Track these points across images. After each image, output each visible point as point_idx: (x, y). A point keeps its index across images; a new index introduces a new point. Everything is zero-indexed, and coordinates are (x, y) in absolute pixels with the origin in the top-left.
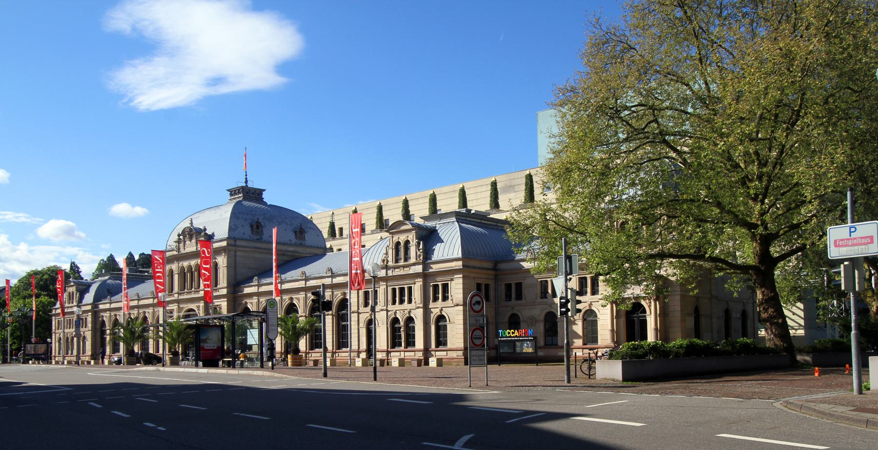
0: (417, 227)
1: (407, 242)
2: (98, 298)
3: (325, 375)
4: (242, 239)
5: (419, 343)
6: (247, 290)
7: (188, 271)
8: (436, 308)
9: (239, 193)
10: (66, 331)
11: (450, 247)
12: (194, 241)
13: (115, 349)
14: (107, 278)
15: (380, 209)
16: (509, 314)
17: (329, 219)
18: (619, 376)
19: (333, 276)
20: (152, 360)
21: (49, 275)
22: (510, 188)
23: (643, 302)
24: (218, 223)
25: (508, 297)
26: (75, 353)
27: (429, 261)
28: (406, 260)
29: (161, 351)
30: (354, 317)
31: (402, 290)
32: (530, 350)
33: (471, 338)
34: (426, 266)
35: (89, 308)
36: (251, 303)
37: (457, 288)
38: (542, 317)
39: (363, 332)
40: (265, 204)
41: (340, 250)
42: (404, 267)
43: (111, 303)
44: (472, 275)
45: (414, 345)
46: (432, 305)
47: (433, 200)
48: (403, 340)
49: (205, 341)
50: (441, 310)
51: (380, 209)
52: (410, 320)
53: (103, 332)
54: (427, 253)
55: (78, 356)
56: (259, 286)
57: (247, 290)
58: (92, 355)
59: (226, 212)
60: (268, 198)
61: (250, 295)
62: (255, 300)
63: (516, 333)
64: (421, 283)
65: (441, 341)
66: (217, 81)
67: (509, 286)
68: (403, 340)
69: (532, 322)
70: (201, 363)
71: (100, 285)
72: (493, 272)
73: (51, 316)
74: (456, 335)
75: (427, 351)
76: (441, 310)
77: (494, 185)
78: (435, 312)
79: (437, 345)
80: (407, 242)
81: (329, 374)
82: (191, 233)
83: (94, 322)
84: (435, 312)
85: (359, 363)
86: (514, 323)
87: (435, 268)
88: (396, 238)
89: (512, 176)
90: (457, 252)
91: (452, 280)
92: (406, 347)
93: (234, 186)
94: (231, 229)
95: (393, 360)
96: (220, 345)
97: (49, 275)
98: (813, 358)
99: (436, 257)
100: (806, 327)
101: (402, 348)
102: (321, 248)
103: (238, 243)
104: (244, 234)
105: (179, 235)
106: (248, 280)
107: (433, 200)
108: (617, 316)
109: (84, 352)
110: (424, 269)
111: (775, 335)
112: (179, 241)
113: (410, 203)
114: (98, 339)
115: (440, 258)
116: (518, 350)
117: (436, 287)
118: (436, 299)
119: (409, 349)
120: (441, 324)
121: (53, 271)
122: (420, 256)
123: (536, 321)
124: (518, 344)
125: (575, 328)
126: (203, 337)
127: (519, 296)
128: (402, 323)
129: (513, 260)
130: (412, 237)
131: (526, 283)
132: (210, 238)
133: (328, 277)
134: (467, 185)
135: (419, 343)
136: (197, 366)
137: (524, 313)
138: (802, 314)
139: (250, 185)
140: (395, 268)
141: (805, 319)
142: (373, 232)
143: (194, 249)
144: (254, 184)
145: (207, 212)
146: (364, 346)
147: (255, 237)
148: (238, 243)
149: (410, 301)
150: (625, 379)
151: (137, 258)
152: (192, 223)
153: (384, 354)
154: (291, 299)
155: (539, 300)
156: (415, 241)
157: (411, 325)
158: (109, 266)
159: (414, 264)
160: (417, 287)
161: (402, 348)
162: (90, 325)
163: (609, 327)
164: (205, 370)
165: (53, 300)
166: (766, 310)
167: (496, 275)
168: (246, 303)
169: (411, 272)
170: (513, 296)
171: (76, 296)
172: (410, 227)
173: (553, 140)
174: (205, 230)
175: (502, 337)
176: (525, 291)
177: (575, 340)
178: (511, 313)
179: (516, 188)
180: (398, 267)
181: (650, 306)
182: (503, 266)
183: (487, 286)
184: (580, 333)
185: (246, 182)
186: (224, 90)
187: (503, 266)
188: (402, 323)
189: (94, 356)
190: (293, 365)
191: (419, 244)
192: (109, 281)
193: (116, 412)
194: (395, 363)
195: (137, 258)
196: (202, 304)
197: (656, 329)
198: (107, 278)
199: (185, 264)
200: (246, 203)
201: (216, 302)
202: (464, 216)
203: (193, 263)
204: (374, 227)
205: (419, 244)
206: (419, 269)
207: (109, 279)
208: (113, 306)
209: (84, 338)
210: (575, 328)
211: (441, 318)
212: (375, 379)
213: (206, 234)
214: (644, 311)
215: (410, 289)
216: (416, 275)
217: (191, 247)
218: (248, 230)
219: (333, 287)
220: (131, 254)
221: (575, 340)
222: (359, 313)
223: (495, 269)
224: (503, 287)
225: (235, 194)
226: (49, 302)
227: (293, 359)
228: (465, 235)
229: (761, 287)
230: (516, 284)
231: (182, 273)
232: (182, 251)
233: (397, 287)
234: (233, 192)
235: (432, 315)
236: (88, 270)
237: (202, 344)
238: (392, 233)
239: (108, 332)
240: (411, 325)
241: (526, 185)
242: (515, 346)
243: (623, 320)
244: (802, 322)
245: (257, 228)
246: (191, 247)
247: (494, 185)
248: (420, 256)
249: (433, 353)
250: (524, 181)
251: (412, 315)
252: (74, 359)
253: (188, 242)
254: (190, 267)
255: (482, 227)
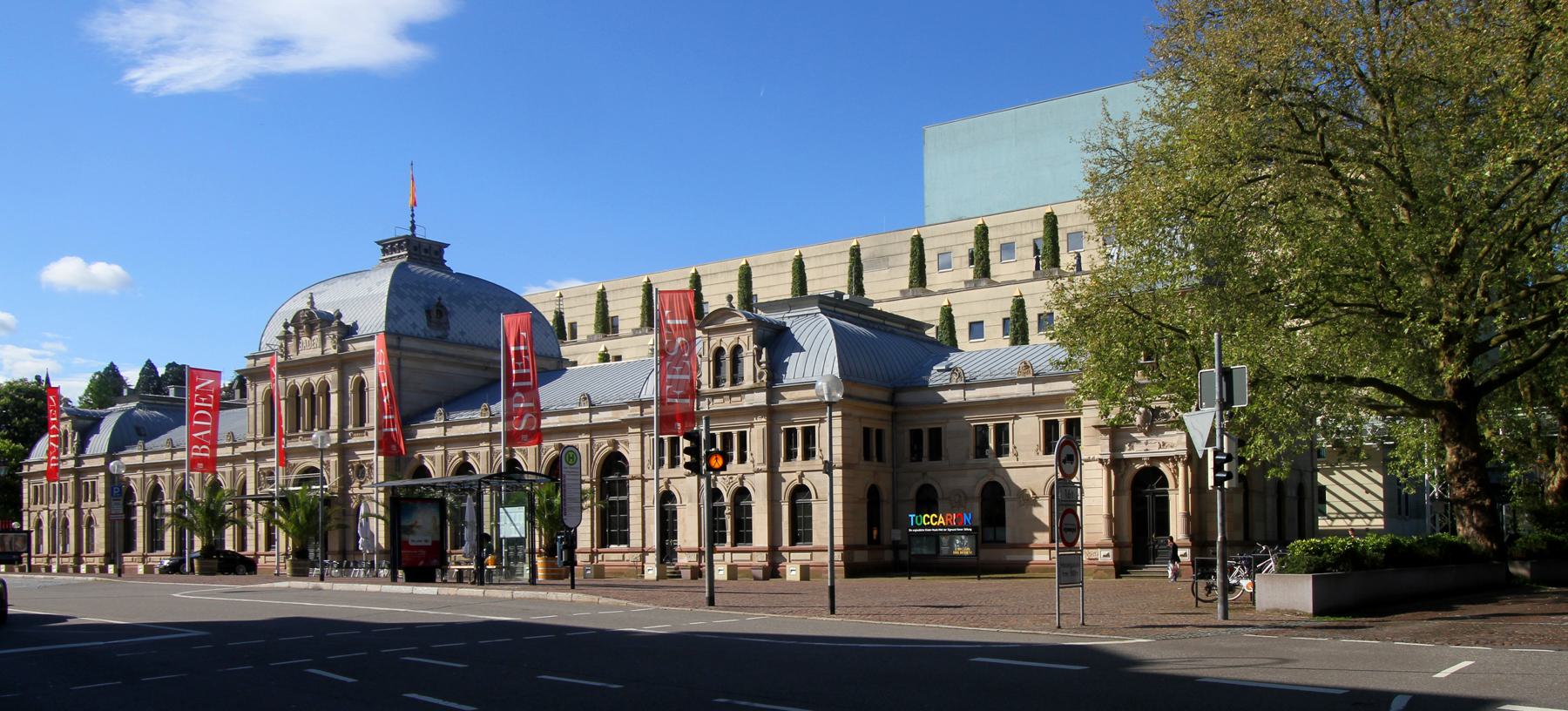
0: (758, 323)
1: (737, 349)
2: (117, 446)
3: (711, 602)
4: (412, 336)
5: (760, 536)
6: (423, 434)
7: (305, 395)
8: (791, 473)
9: (401, 248)
10: (54, 507)
11: (817, 362)
12: (317, 337)
13: (155, 544)
14: (133, 405)
15: (602, 296)
16: (917, 485)
17: (554, 307)
18: (1308, 606)
19: (593, 409)
20: (239, 565)
21: (12, 397)
22: (882, 260)
23: (1163, 467)
24: (365, 300)
25: (916, 455)
26: (71, 549)
27: (778, 385)
28: (734, 382)
29: (251, 549)
30: (634, 487)
31: (727, 438)
32: (967, 551)
33: (1060, 528)
34: (773, 395)
35: (101, 462)
36: (432, 458)
37: (831, 437)
38: (978, 492)
39: (652, 515)
40: (449, 271)
41: (618, 358)
42: (731, 394)
43: (145, 454)
44: (858, 413)
45: (749, 540)
46: (783, 466)
47: (746, 276)
48: (729, 530)
49: (409, 530)
50: (801, 476)
51: (602, 296)
52: (742, 493)
53: (130, 511)
54: (775, 370)
55: (78, 558)
56: (447, 425)
57: (423, 434)
58: (107, 555)
59: (379, 283)
60: (456, 260)
61: (430, 443)
62: (438, 452)
63: (941, 521)
64: (764, 426)
65: (801, 531)
66: (277, 45)
67: (916, 435)
68: (729, 530)
69: (958, 501)
70: (401, 573)
71: (118, 423)
72: (889, 409)
73: (21, 478)
74: (829, 520)
75: (774, 550)
76: (801, 476)
77: (855, 252)
78: (790, 480)
79: (794, 539)
80: (737, 349)
81: (717, 597)
82: (311, 321)
83: (110, 491)
84: (790, 480)
85: (651, 573)
86: (927, 501)
87: (790, 397)
88: (715, 341)
89: (884, 238)
90: (832, 367)
91: (1016, 417)
92: (734, 544)
93: (389, 234)
94: (390, 316)
95: (789, 567)
96: (437, 538)
97: (12, 397)
98: (1531, 571)
99: (790, 377)
100: (1387, 515)
101: (728, 545)
102: (552, 357)
103: (405, 343)
104: (414, 326)
105: (286, 325)
106: (424, 414)
107: (746, 276)
108: (1115, 492)
109: (90, 548)
110: (770, 399)
111: (1477, 528)
112: (286, 337)
113: (703, 282)
114: (119, 527)
115: (799, 380)
116: (944, 550)
117: (791, 434)
118: (790, 456)
119: (740, 547)
120: (799, 501)
121: (19, 390)
122: (761, 375)
123: (966, 498)
124: (944, 539)
125: (1036, 512)
126: (405, 522)
127: (936, 453)
128: (727, 500)
129: (925, 386)
130: (746, 339)
131: (949, 428)
132: (349, 332)
133: (583, 411)
134: (807, 252)
135: (760, 536)
136: (394, 579)
137: (945, 484)
138: (1380, 491)
139: (419, 234)
140: (713, 396)
141: (1385, 500)
142: (590, 339)
143: (317, 352)
144: (429, 232)
145: (339, 281)
146: (653, 541)
147: (434, 333)
148: (405, 343)
149: (742, 459)
150: (1318, 611)
151: (161, 371)
152: (312, 303)
153: (694, 557)
154: (465, 455)
155: (972, 460)
156: (753, 347)
157: (743, 503)
158: (108, 385)
159: (751, 390)
160: (757, 434)
161: (728, 545)
162: (101, 496)
163: (1105, 511)
164: (407, 589)
165: (20, 446)
166: (1463, 482)
167: (894, 414)
168: (421, 457)
169: (745, 405)
170: (926, 451)
171: (73, 440)
172: (744, 320)
173: (1089, 156)
174: (340, 316)
175: (916, 526)
176: (947, 443)
177: (1036, 535)
178: (921, 482)
179: (891, 261)
180: (720, 395)
181: (1175, 474)
182: (906, 397)
183: (879, 433)
184: (1047, 522)
185: (413, 228)
186: (291, 63)
187: (906, 397)
188: (727, 500)
189: (111, 556)
190: (549, 576)
191: (759, 353)
192: (138, 412)
193: (350, 680)
194: (721, 573)
195: (161, 371)
196: (333, 459)
197: (1187, 515)
198: (133, 405)
199: (300, 381)
200: (414, 268)
201: (363, 455)
202: (848, 309)
203: (315, 379)
204: (637, 323)
205: (759, 353)
206: (760, 398)
207: (139, 406)
208: (150, 459)
209: (90, 520)
210: (1036, 512)
211: (800, 490)
212: (833, 612)
213: (341, 324)
214: (1165, 483)
215: (742, 436)
216: (754, 411)
217: (310, 348)
218: (422, 322)
219: (593, 429)
220: (149, 364)
221: (1036, 535)
222: (644, 480)
223: (892, 402)
224: (907, 435)
225: (393, 250)
226: (14, 451)
227: (547, 565)
228: (844, 340)
229: (1456, 440)
230: (931, 430)
231: (294, 397)
232: (293, 356)
233: (717, 432)
234: (388, 247)
235: (784, 486)
236: (74, 388)
237: (404, 537)
238: (708, 332)
239: (168, 508)
240: (743, 503)
241: (913, 255)
242: (938, 544)
243: (1126, 498)
244: (1380, 506)
245: (438, 314)
246: (310, 348)
247: (855, 252)
248: (761, 375)
249: (785, 555)
250: (908, 247)
251: (746, 485)
252: (69, 561)
253: (304, 339)
254: (309, 388)
255: (866, 327)
